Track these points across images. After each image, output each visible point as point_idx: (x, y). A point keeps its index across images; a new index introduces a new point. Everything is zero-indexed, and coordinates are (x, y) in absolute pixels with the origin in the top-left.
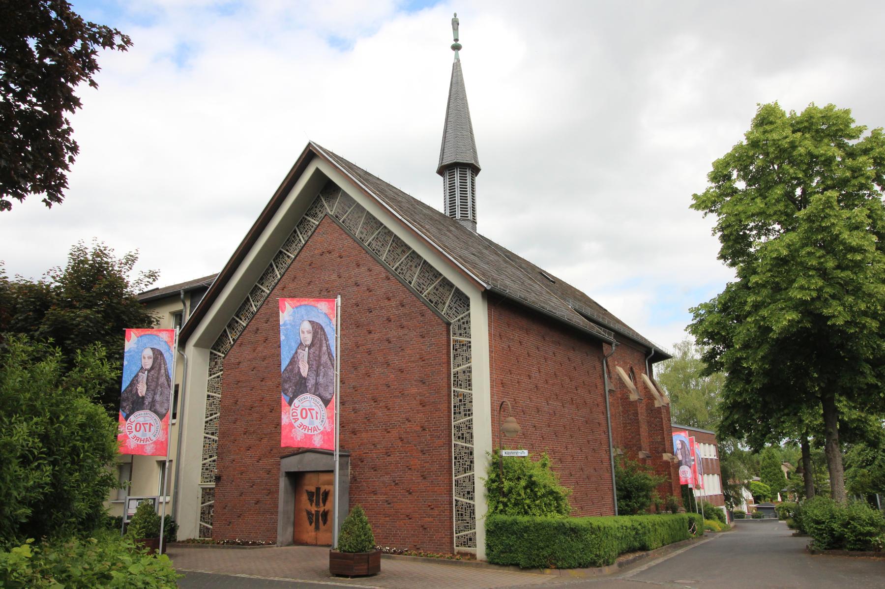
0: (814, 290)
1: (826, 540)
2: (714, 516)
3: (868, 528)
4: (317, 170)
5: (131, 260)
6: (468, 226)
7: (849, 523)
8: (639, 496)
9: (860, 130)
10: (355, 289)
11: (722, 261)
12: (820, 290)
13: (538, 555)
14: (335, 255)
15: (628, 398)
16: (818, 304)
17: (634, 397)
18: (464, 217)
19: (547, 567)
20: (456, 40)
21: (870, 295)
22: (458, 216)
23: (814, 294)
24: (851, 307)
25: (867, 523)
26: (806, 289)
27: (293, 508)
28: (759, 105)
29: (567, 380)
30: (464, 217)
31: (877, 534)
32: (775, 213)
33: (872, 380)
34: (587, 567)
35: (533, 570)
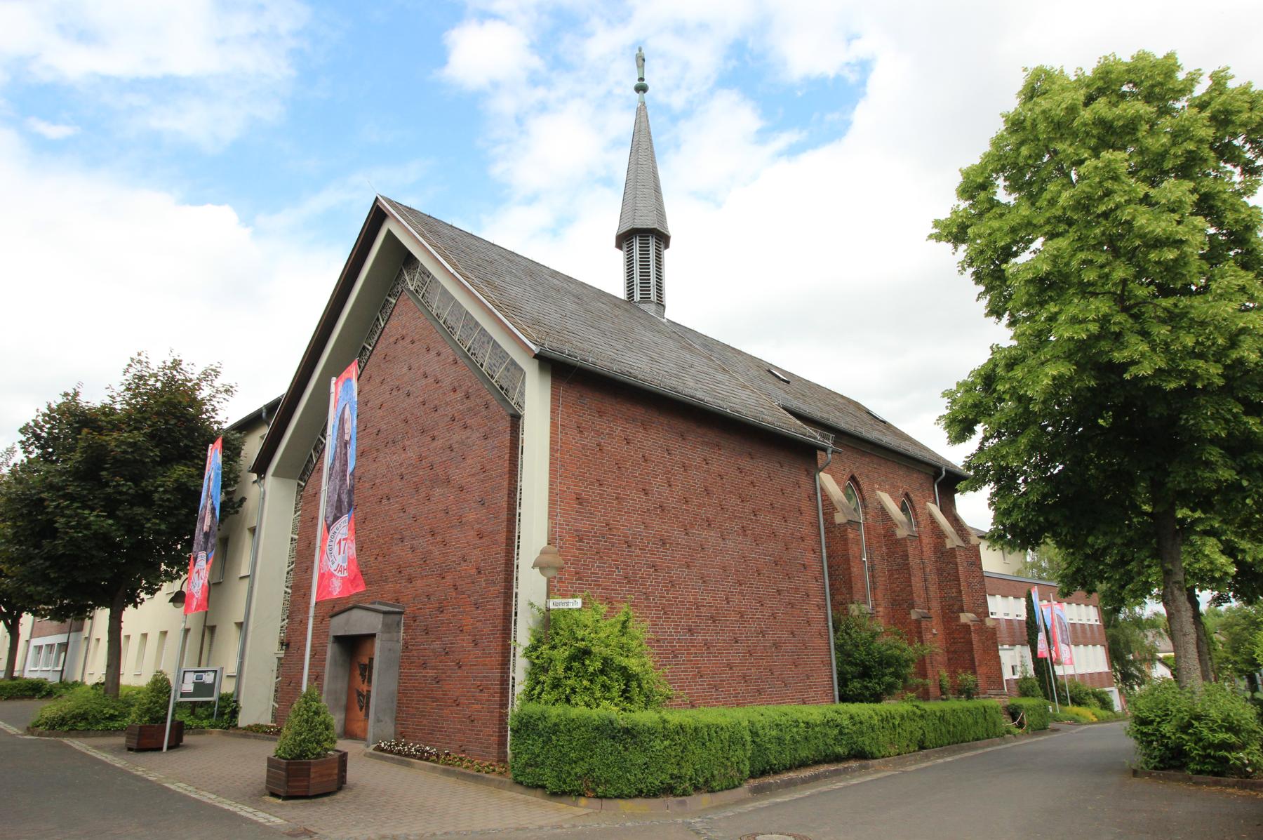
0: (1094, 320)
1: (1156, 753)
2: (1094, 700)
3: (1221, 736)
4: (389, 232)
5: (208, 375)
6: (650, 309)
7: (1191, 725)
8: (884, 675)
9: (1192, 80)
10: (424, 382)
11: (993, 318)
12: (1104, 320)
13: (570, 774)
14: (408, 340)
15: (893, 534)
16: (1104, 345)
17: (901, 533)
18: (645, 298)
19: (581, 795)
20: (642, 79)
21: (1203, 324)
22: (637, 297)
23: (1094, 328)
24: (1167, 345)
25: (1220, 727)
26: (1080, 322)
27: (346, 686)
28: (1025, 69)
29: (734, 500)
30: (645, 298)
31: (1243, 747)
32: (1048, 221)
33: (1226, 474)
34: (655, 796)
35: (565, 799)
